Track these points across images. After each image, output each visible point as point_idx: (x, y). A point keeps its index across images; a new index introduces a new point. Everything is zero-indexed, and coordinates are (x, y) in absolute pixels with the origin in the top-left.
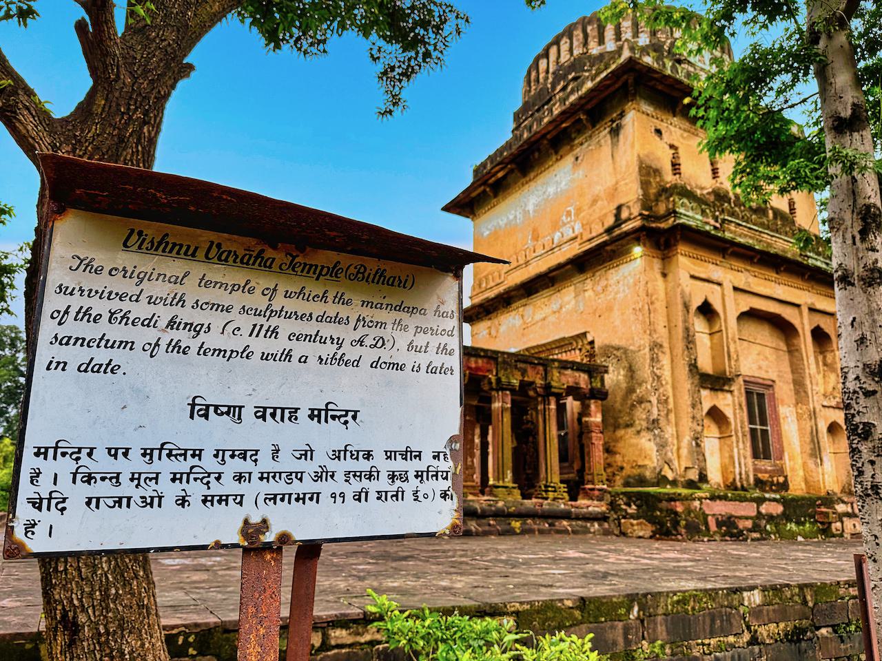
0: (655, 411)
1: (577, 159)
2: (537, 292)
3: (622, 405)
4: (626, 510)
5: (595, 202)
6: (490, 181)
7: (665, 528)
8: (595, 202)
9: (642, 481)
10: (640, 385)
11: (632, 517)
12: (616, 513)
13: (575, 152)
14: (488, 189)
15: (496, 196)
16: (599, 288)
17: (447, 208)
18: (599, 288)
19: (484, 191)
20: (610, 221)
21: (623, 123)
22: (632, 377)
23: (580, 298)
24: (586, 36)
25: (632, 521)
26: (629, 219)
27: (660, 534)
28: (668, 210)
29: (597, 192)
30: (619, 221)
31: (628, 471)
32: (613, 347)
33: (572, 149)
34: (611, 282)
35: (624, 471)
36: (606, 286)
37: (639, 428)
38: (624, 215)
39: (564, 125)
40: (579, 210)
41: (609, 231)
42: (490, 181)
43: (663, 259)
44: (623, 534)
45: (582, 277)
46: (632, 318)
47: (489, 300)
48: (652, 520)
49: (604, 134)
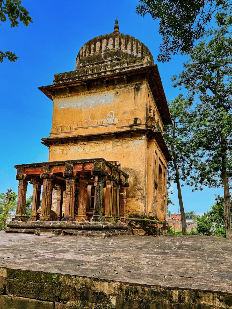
0: (145, 193)
1: (117, 93)
3: (131, 190)
4: (135, 226)
6: (70, 85)
7: (150, 232)
8: (125, 113)
9: (137, 216)
10: (140, 184)
11: (137, 228)
12: (131, 227)
13: (116, 90)
14: (67, 88)
15: (70, 92)
16: (124, 146)
17: (41, 89)
19: (65, 88)
20: (132, 123)
21: (141, 87)
22: (136, 180)
23: (115, 148)
24: (120, 43)
25: (137, 229)
26: (141, 124)
27: (148, 234)
28: (151, 125)
29: (126, 110)
30: (135, 124)
31: (131, 212)
32: (129, 169)
33: (115, 88)
35: (130, 212)
36: (128, 146)
37: (138, 198)
38: (138, 122)
39: (115, 77)
41: (131, 126)
42: (70, 85)
43: (148, 142)
45: (117, 140)
47: (51, 139)
48: (145, 230)
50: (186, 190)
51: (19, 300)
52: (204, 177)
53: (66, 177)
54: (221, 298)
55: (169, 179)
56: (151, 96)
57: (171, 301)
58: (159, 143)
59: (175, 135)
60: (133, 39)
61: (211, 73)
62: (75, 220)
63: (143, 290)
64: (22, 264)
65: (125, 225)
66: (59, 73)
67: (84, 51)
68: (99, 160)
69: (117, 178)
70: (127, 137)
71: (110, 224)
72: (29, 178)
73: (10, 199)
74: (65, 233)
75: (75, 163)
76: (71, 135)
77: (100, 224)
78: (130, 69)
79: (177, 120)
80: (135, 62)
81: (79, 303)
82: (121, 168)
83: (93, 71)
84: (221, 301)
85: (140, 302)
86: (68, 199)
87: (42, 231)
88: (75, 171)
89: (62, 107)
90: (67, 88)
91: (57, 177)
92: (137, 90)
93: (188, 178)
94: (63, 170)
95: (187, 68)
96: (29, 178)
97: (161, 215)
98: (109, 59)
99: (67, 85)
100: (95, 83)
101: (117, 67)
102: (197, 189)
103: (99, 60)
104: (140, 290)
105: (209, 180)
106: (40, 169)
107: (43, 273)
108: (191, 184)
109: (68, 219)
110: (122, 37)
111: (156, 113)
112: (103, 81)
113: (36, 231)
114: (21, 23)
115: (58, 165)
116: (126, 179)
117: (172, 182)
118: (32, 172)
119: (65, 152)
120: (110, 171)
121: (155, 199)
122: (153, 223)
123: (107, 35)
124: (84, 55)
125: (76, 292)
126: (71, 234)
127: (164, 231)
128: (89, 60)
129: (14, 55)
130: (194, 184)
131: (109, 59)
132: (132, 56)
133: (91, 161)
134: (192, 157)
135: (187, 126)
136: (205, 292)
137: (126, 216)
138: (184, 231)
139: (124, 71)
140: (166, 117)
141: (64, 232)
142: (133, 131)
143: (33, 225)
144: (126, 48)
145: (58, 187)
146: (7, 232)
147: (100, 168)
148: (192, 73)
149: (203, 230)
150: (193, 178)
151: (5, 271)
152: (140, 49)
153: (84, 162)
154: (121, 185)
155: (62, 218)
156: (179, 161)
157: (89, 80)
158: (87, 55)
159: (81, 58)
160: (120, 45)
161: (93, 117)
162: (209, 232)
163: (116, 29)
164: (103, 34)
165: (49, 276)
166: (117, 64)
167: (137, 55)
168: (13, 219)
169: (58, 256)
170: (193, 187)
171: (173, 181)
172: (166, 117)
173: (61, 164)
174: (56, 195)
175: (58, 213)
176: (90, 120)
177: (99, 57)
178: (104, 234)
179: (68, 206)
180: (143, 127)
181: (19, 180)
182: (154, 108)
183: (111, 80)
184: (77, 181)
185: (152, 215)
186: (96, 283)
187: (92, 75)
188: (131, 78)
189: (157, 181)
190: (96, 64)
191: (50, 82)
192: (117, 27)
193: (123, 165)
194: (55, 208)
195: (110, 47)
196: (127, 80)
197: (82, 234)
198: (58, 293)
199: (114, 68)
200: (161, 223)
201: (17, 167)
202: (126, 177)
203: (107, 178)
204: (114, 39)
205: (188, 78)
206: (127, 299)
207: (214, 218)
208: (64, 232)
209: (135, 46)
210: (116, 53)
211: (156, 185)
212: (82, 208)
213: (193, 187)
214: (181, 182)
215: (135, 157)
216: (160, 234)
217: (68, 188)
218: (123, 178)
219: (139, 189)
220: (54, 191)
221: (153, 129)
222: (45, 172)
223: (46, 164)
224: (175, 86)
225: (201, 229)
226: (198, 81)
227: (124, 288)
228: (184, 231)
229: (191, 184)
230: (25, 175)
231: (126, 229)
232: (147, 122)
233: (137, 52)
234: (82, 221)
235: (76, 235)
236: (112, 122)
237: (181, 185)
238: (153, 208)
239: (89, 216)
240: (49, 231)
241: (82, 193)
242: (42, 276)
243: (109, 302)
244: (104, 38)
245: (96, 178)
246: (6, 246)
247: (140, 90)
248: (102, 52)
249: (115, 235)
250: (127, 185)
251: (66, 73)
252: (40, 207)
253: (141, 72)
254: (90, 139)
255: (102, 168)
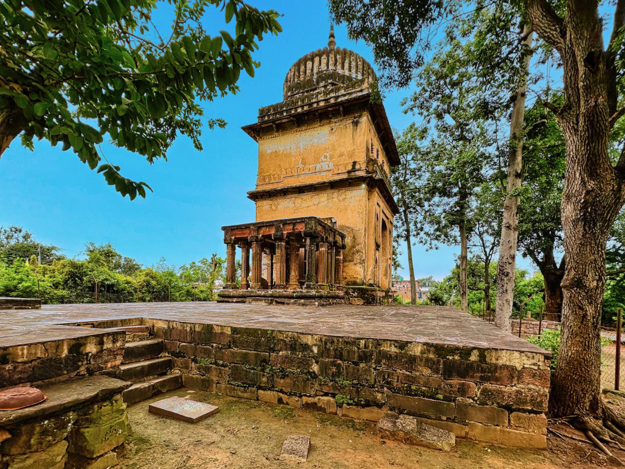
2: (388, 203)
5: (341, 155)
6: (277, 122)
9: (355, 283)
11: (355, 297)
14: (274, 126)
16: (341, 198)
17: (244, 128)
18: (341, 198)
19: (272, 126)
20: (350, 168)
24: (336, 61)
26: (359, 170)
30: (354, 169)
31: (349, 279)
34: (347, 197)
38: (357, 167)
40: (332, 157)
41: (349, 172)
42: (277, 122)
44: (350, 303)
45: (332, 191)
46: (358, 215)
47: (258, 192)
48: (363, 298)
49: (349, 122)
50: (418, 249)
51: (242, 353)
52: (441, 233)
53: (276, 239)
54: (396, 344)
55: (398, 236)
56: (373, 130)
57: (359, 348)
58: (382, 192)
59: (407, 178)
60: (351, 53)
61: (452, 92)
62: (287, 288)
63: (338, 341)
64: (241, 324)
65: (341, 293)
66: (264, 106)
67: (292, 74)
68: (310, 218)
69: (331, 239)
70: (344, 187)
71: (324, 292)
72: (237, 241)
73: (216, 265)
74: (277, 303)
75: (285, 222)
76: (279, 187)
77: (313, 292)
78: (346, 98)
79: (409, 157)
80: (353, 86)
81: (289, 352)
82: (337, 227)
83: (303, 101)
84: (396, 347)
85: (335, 350)
86: (279, 264)
87: (253, 300)
88: (285, 232)
89: (269, 151)
90: (274, 126)
91: (266, 240)
92: (356, 124)
93: (422, 234)
94: (273, 232)
95: (420, 88)
96: (237, 241)
97: (384, 283)
98: (322, 84)
99: (274, 121)
100: (306, 118)
101: (332, 95)
102: (431, 248)
103: (309, 86)
104: (335, 340)
105: (446, 236)
106: (247, 231)
107: (260, 329)
108: (424, 242)
109: (279, 287)
110: (338, 52)
111: (380, 153)
112: (315, 115)
113: (247, 299)
114: (230, 93)
115: (267, 226)
116: (342, 239)
117: (402, 241)
118: (239, 235)
119: (273, 207)
120: (323, 231)
121: (376, 262)
122: (373, 291)
123: (319, 51)
124: (292, 80)
125: (286, 344)
126: (283, 303)
127: (386, 300)
128: (298, 86)
129: (223, 121)
130: (428, 242)
131: (322, 84)
132: (350, 79)
133: (302, 220)
134: (427, 207)
135: (421, 165)
136: (385, 340)
137: (343, 284)
138: (414, 301)
139: (340, 100)
140: (393, 158)
141: (276, 301)
142: (351, 179)
143: (244, 293)
144: (343, 68)
145: (267, 251)
146: (219, 302)
147: (311, 229)
148: (427, 94)
149: (436, 300)
150: (427, 234)
151: (229, 329)
152: (360, 67)
153: (294, 222)
154: (337, 248)
155: (273, 286)
156: (410, 212)
157: (299, 114)
158: (296, 80)
159: (289, 83)
160: (335, 64)
161: (304, 163)
162: (442, 301)
163: (332, 39)
164: (315, 50)
165: (265, 332)
166: (332, 91)
167: (357, 76)
168: (224, 288)
169: (271, 319)
170: (427, 246)
171: (403, 239)
172: (393, 158)
173: (270, 224)
174: (265, 260)
175: (269, 281)
176: (301, 166)
177: (310, 81)
178: (317, 303)
179: (279, 273)
180: (362, 174)
181: (227, 244)
182: (377, 145)
183: (325, 112)
184: (287, 243)
185: (371, 282)
186: (302, 336)
187: (302, 107)
188: (349, 109)
189: (380, 241)
190: (307, 92)
191: (254, 120)
192: (332, 36)
193: (340, 221)
194: (265, 276)
195: (323, 67)
196: (344, 112)
197: (294, 303)
198: (272, 346)
199: (328, 97)
200: (383, 291)
201: (224, 228)
202: (343, 237)
203: (320, 239)
204: (328, 56)
205: (422, 100)
206: (325, 348)
207: (453, 284)
208: (276, 301)
209: (353, 64)
210: (330, 76)
211: (378, 246)
212: (294, 274)
213: (427, 246)
214: (413, 239)
215: (353, 211)
216: (381, 304)
217: (278, 251)
218: (339, 238)
219: (358, 251)
220: (264, 255)
221: (374, 175)
222: (254, 234)
223: (254, 224)
224: (406, 113)
225: (433, 297)
226: (435, 104)
227: (323, 340)
228: (414, 301)
229: (424, 242)
230: (233, 237)
231: (343, 298)
232: (367, 167)
233: (357, 72)
234: (295, 289)
235: (288, 304)
236: (327, 168)
237: (412, 243)
238: (374, 275)
239: (302, 284)
240: (261, 300)
241: (293, 258)
242: (259, 332)
243: (312, 351)
244: (317, 55)
245: (308, 241)
246: (223, 313)
247: (359, 125)
248: (313, 75)
249: (330, 304)
250: (344, 247)
251: (272, 106)
252: (250, 274)
253: (360, 101)
254: (301, 190)
255: (314, 228)
